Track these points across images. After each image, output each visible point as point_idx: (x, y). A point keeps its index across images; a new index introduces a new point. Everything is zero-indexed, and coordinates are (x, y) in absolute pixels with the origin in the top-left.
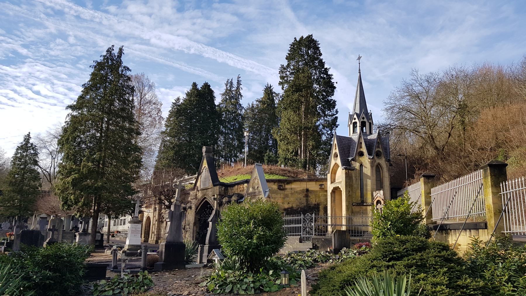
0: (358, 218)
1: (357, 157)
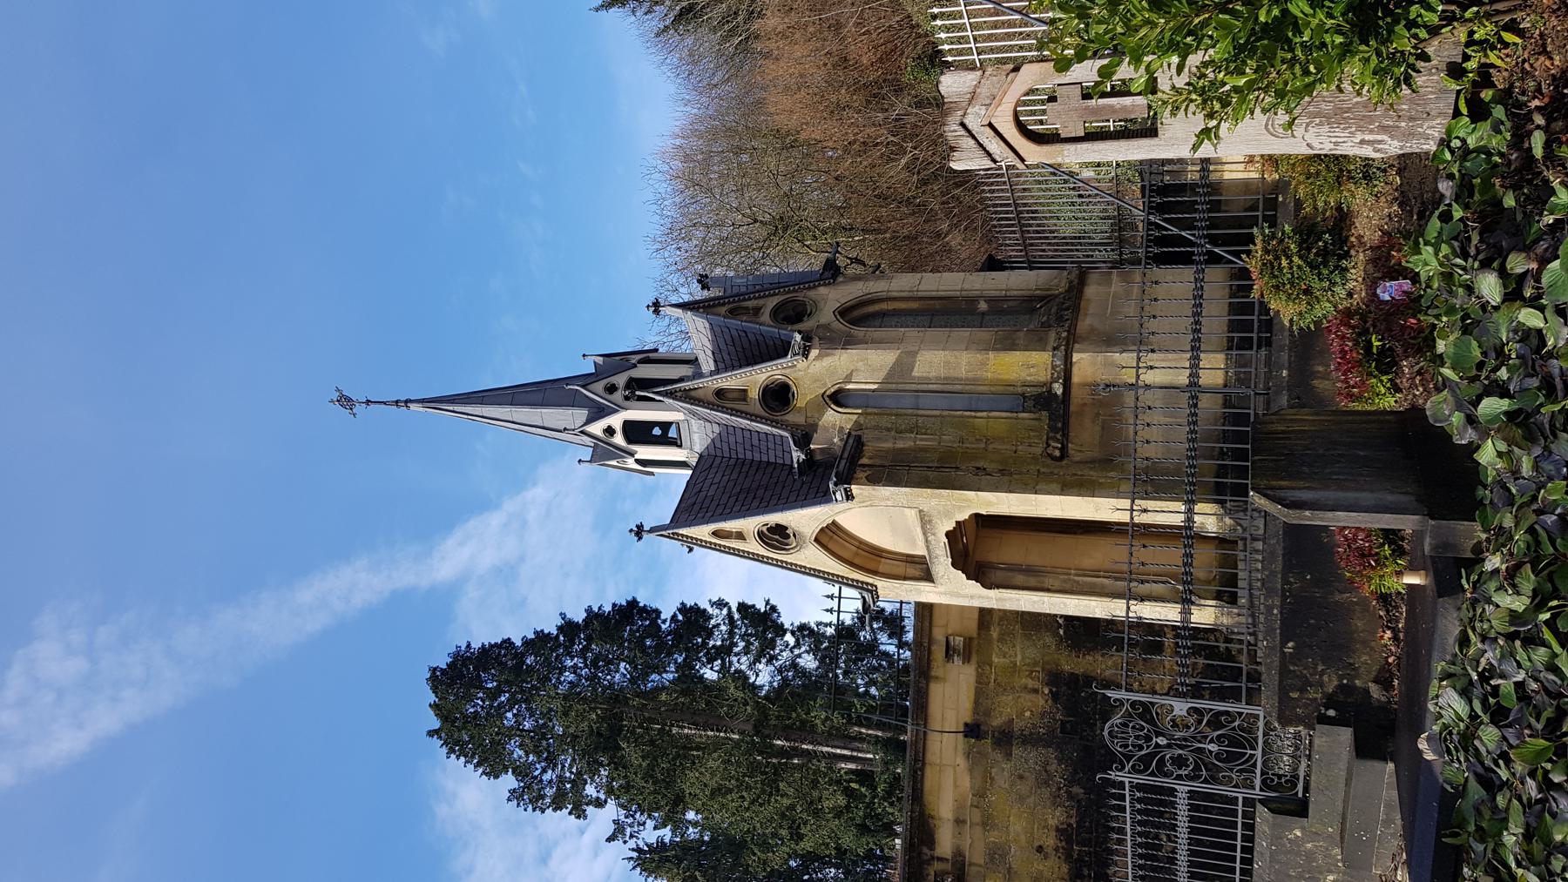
0: (1144, 433)
1: (791, 418)
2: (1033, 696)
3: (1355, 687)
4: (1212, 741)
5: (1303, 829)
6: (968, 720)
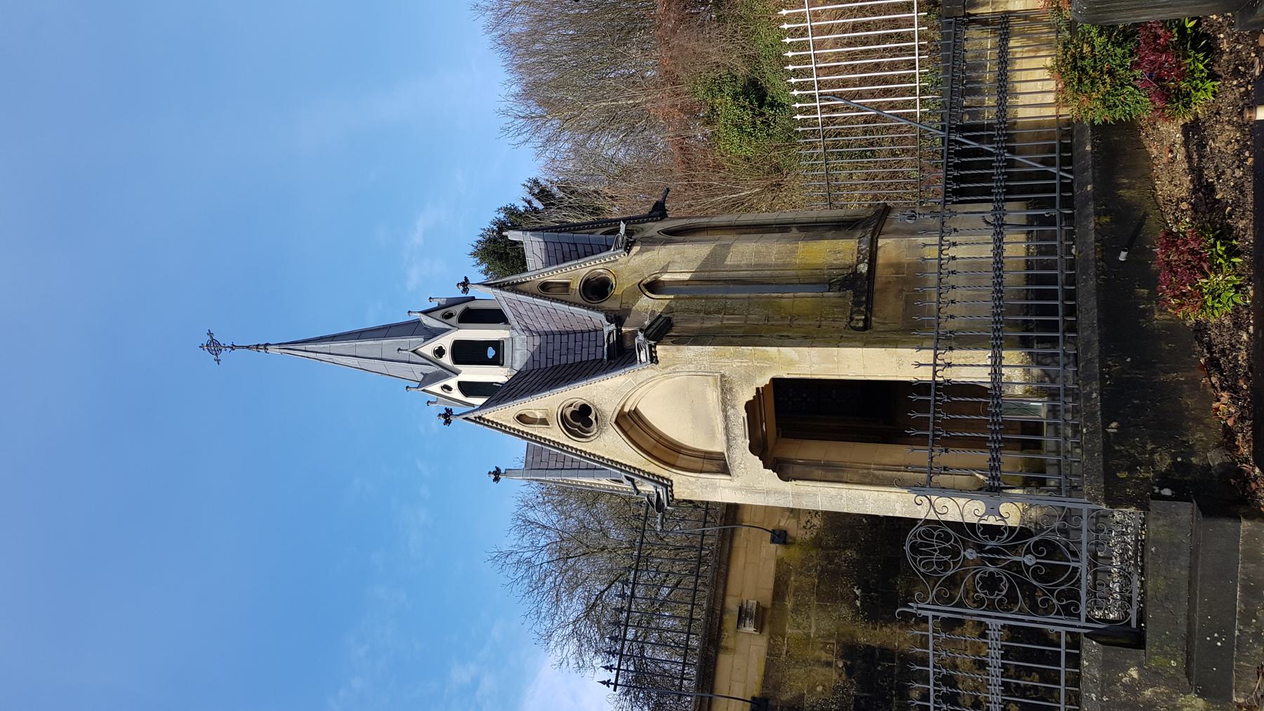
2: (826, 670)
3: (1191, 464)
4: (1028, 552)
5: (1140, 666)
6: (756, 694)
